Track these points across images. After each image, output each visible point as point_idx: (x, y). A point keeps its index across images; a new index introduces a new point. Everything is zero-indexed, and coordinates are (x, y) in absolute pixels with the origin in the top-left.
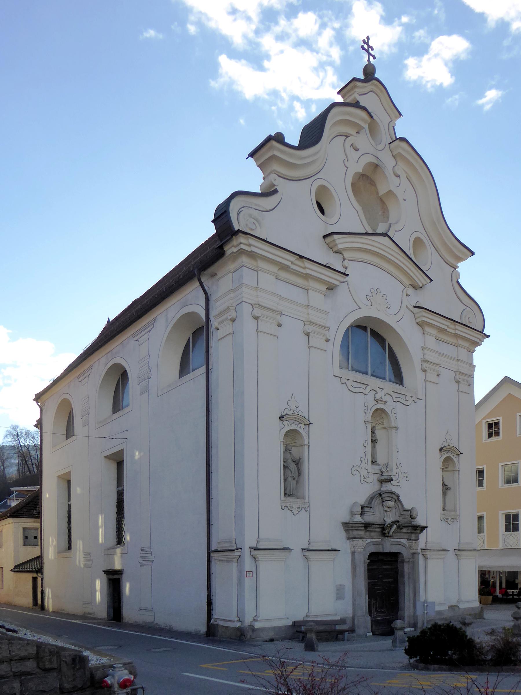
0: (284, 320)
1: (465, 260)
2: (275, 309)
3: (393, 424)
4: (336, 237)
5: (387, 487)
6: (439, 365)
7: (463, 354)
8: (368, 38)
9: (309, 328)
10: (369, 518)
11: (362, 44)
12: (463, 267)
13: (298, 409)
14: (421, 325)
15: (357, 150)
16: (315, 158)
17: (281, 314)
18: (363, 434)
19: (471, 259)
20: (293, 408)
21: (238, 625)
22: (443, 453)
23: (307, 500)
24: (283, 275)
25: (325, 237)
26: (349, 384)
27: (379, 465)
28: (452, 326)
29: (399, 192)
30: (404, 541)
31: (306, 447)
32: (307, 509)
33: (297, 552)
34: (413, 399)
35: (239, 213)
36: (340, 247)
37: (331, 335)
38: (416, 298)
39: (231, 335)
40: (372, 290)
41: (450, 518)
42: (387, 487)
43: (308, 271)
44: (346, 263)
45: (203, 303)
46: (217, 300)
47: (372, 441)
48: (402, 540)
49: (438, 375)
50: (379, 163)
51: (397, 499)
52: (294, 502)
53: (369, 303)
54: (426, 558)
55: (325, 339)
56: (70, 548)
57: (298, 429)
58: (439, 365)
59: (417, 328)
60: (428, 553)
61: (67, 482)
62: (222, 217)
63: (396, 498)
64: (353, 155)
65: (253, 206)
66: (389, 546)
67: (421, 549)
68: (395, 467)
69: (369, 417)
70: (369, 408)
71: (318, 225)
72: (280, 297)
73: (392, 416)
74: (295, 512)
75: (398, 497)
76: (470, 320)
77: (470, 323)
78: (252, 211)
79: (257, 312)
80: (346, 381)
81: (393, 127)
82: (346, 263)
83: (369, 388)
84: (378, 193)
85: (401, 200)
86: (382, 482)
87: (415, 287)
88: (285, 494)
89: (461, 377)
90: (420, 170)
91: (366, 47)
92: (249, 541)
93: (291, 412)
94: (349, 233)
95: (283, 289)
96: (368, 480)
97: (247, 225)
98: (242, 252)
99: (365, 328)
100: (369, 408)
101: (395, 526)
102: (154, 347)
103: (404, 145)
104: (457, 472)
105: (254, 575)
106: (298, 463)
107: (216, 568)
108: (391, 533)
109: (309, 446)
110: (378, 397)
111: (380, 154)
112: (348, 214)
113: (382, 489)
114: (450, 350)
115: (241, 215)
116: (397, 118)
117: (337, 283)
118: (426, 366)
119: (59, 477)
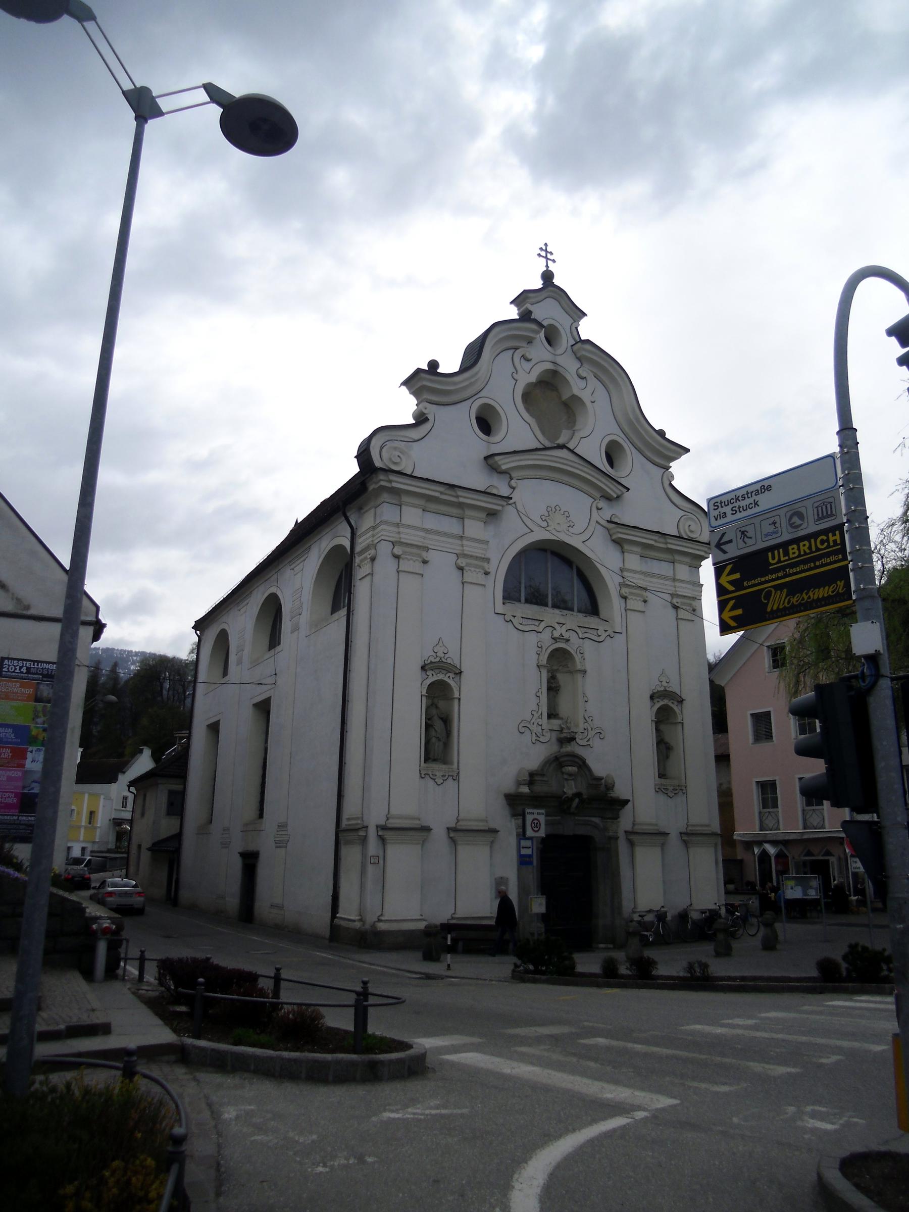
0: (430, 556)
1: (677, 459)
2: (420, 544)
3: (579, 667)
4: (497, 458)
5: (568, 748)
6: (645, 589)
7: (682, 571)
8: (546, 245)
9: (462, 562)
10: (539, 789)
11: (539, 252)
12: (676, 467)
13: (447, 656)
14: (619, 543)
15: (528, 360)
16: (473, 380)
17: (427, 549)
18: (536, 681)
19: (685, 457)
20: (440, 654)
21: (358, 925)
22: (655, 701)
23: (455, 765)
24: (433, 506)
25: (486, 458)
26: (515, 621)
27: (562, 719)
28: (662, 540)
29: (585, 396)
30: (596, 820)
31: (456, 702)
32: (456, 778)
33: (674, 839)
34: (607, 633)
35: (382, 448)
36: (504, 467)
37: (492, 568)
38: (608, 512)
39: (369, 578)
40: (548, 509)
41: (671, 788)
42: (568, 748)
43: (461, 500)
44: (513, 483)
45: (349, 535)
46: (360, 536)
47: (549, 689)
48: (593, 819)
49: (645, 601)
50: (560, 369)
51: (582, 764)
52: (438, 769)
53: (544, 524)
54: (632, 844)
55: (483, 571)
56: (261, 816)
57: (446, 679)
58: (645, 589)
59: (610, 544)
60: (388, 835)
61: (214, 728)
62: (364, 455)
63: (580, 763)
64: (527, 366)
65: (399, 439)
66: (572, 827)
67: (626, 832)
68: (581, 721)
69: (544, 659)
70: (544, 649)
71: (477, 445)
72: (427, 531)
73: (577, 658)
74: (440, 781)
75: (584, 761)
76: (691, 528)
77: (692, 532)
78: (397, 444)
79: (398, 551)
80: (512, 618)
81: (577, 328)
82: (513, 483)
83: (543, 625)
84: (560, 398)
85: (588, 404)
86: (562, 741)
87: (608, 498)
88: (427, 760)
89: (679, 600)
90: (611, 370)
91: (543, 254)
92: (375, 817)
93: (438, 659)
94: (515, 452)
95: (432, 522)
96: (542, 739)
97: (390, 459)
98: (383, 488)
99: (545, 550)
100: (544, 649)
101: (577, 800)
102: (300, 585)
103: (588, 347)
104: (680, 725)
105: (381, 862)
106: (446, 721)
107: (344, 851)
108: (572, 810)
109: (459, 699)
110: (556, 634)
111: (559, 360)
112: (518, 431)
113: (562, 750)
114: (664, 568)
115: (384, 450)
116: (581, 318)
117: (499, 508)
118: (625, 591)
119: (208, 726)
